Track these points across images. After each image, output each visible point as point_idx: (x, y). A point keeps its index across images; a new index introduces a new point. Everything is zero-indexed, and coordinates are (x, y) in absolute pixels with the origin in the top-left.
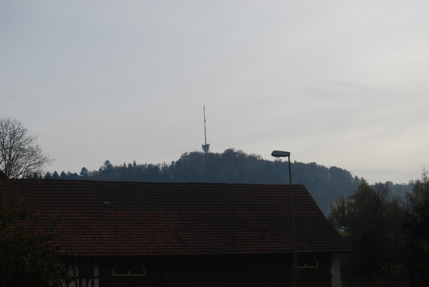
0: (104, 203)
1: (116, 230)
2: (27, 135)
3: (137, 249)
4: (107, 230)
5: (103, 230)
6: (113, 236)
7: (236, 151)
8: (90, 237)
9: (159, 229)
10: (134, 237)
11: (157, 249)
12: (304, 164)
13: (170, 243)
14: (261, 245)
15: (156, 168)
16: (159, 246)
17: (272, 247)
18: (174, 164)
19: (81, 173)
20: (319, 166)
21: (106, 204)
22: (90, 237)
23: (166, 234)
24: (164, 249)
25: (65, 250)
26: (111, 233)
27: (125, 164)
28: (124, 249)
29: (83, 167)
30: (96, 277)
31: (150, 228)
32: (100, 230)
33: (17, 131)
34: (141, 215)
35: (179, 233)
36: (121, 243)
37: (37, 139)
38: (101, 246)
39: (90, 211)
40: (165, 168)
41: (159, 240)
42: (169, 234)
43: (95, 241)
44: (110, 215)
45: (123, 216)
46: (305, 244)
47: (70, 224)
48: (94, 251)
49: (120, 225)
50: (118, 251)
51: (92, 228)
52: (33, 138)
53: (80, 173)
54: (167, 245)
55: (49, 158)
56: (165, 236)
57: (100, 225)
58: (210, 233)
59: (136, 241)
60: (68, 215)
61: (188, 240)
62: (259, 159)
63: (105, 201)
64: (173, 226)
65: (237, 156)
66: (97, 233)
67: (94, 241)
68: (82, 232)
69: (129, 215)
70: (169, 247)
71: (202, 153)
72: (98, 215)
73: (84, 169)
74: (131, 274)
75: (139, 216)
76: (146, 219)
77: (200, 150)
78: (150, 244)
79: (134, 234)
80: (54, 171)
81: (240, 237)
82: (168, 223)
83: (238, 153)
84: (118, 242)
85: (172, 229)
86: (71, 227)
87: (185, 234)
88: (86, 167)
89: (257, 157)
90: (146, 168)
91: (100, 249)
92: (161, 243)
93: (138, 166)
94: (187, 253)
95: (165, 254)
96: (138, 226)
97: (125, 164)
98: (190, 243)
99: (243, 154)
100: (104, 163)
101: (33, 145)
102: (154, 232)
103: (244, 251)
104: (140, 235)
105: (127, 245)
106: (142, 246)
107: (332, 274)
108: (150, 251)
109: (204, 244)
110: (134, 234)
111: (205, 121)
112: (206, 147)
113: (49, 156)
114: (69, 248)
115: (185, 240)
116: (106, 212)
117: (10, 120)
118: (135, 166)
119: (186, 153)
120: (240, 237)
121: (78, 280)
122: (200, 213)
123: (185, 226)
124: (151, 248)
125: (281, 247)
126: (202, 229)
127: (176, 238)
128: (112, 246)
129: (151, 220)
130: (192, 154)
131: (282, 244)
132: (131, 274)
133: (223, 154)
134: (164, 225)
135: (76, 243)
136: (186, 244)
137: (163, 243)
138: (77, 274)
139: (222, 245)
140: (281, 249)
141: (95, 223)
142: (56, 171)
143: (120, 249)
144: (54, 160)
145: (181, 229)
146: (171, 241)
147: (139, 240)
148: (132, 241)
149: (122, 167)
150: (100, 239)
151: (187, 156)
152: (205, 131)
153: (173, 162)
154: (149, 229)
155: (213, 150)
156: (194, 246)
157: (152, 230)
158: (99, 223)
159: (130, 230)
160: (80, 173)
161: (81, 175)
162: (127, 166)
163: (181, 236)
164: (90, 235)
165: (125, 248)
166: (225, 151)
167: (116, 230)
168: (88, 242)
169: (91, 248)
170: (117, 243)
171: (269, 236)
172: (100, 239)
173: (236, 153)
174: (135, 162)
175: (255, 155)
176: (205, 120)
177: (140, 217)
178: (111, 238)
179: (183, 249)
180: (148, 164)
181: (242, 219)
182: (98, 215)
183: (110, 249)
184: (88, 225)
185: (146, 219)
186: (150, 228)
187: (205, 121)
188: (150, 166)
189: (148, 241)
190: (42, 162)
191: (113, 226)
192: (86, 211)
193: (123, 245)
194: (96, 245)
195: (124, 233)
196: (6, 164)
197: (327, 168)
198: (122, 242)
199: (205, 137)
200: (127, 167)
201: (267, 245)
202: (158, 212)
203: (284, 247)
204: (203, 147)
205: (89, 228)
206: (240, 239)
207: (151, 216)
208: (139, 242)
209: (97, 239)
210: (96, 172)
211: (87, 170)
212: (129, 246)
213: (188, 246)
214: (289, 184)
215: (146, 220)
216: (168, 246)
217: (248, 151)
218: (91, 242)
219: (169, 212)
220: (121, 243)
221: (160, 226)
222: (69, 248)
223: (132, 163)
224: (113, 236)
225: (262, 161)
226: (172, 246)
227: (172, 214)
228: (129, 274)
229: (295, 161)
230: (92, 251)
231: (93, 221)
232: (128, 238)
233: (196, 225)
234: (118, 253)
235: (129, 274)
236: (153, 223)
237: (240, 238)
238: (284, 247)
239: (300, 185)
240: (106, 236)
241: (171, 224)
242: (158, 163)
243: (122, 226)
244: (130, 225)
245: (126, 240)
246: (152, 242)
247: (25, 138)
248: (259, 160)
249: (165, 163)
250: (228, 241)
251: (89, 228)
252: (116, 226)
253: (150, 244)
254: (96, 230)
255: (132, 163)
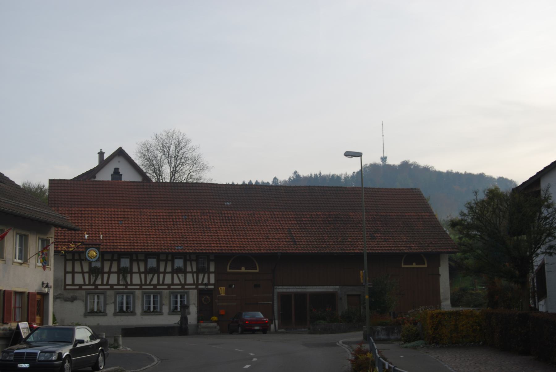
0: (225, 204)
1: (233, 229)
2: (190, 145)
3: (250, 247)
4: (224, 229)
5: (221, 229)
6: (229, 235)
7: (411, 162)
8: (208, 236)
9: (274, 229)
10: (249, 236)
11: (269, 247)
12: (394, 165)
13: (283, 242)
14: (370, 244)
15: (338, 178)
16: (271, 244)
17: (381, 247)
18: (355, 174)
19: (273, 182)
20: (488, 176)
21: (227, 205)
22: (208, 236)
23: (279, 234)
24: (275, 247)
25: (182, 247)
26: (228, 232)
27: (311, 175)
28: (237, 247)
29: (274, 177)
30: (212, 273)
31: (266, 227)
32: (217, 229)
33: (181, 141)
34: (259, 216)
35: (293, 233)
36: (235, 241)
37: (199, 149)
38: (217, 244)
39: (210, 211)
40: (347, 178)
41: (272, 239)
42: (282, 234)
43: (212, 238)
44: (229, 215)
45: (241, 216)
46: (413, 244)
47: (191, 223)
48: (209, 248)
49: (237, 224)
50: (232, 248)
51: (211, 226)
52: (196, 147)
53: (272, 182)
54: (280, 243)
55: (208, 166)
56: (278, 235)
57: (219, 224)
58: (323, 233)
59: (250, 239)
60: (190, 214)
61: (300, 239)
62: (432, 169)
63: (226, 202)
64: (288, 226)
65: (412, 167)
66: (215, 231)
67: (210, 239)
68: (200, 230)
69: (247, 216)
70: (281, 245)
71: (380, 164)
72: (217, 215)
73: (275, 178)
74: (245, 269)
75: (256, 216)
76: (263, 219)
77: (379, 162)
78: (263, 243)
79: (249, 233)
80: (249, 180)
81: (351, 236)
82: (283, 223)
83: (412, 165)
84: (234, 240)
85: (286, 229)
86: (191, 226)
87: (298, 234)
88: (277, 177)
89: (430, 168)
90: (330, 178)
91: (215, 246)
92: (273, 241)
93: (323, 176)
94: (297, 251)
95: (276, 251)
96: (255, 226)
97: (311, 175)
98: (301, 242)
99: (418, 165)
100: (293, 173)
101: (195, 154)
102: (269, 231)
103: (353, 250)
104: (255, 233)
105: (241, 243)
106: (255, 244)
107: (440, 273)
108: (262, 249)
109: (315, 243)
110: (249, 233)
111: (383, 135)
112: (384, 159)
113: (208, 163)
114: (186, 245)
115: (297, 239)
116: (226, 212)
117: (175, 132)
118: (321, 176)
119: (366, 165)
120: (351, 236)
121: (195, 275)
122: (315, 214)
123: (299, 226)
124: (264, 246)
125: (390, 247)
126: (315, 229)
127: (289, 237)
128: (226, 244)
129: (268, 220)
130: (371, 165)
131: (391, 244)
132: (245, 269)
133: (399, 166)
134: (279, 224)
135: (193, 241)
136: (298, 243)
137: (276, 241)
138: (195, 270)
139: (332, 244)
140: (389, 248)
141: (214, 222)
142: (251, 180)
143: (234, 247)
144: (213, 167)
145: (295, 229)
146: (284, 240)
147: (253, 239)
148: (247, 239)
149: (308, 177)
150: (216, 237)
151: (367, 167)
152: (383, 145)
153: (354, 172)
154: (265, 228)
155: (389, 162)
156: (304, 244)
157: (267, 229)
158: (217, 222)
159: (246, 230)
160: (272, 182)
161: (273, 183)
162: (313, 176)
163: (294, 235)
164: (207, 233)
165: (239, 245)
166: (401, 163)
167: (233, 229)
168: (205, 239)
169: (206, 245)
170: (232, 241)
171: (380, 236)
172: (216, 237)
173: (411, 165)
174: (320, 172)
175: (428, 166)
176: (384, 134)
177: (258, 217)
178: (227, 236)
179: (294, 247)
180: (332, 174)
181: (355, 220)
182: (217, 215)
183: (224, 247)
184: (207, 224)
185: (263, 219)
186: (266, 227)
187: (383, 135)
188: (333, 176)
189: (262, 240)
190: (204, 170)
191: (230, 226)
192: (207, 211)
193: (237, 243)
194: (212, 242)
195: (240, 232)
196: (172, 171)
197: (494, 179)
198: (236, 240)
199: (384, 150)
200: (313, 177)
201: (376, 244)
202: (275, 213)
203: (392, 247)
204: (382, 158)
205: (208, 227)
206: (350, 239)
207: (268, 216)
208: (253, 240)
209: (214, 237)
210: (286, 181)
211: (278, 180)
212: (243, 244)
213: (299, 244)
214: (360, 186)
215: (262, 220)
216: (280, 244)
217: (422, 162)
218: (207, 239)
219: (286, 212)
220: (235, 241)
221: (276, 226)
222: (186, 245)
223: (318, 173)
224: (229, 235)
225: (435, 171)
226: (284, 244)
227: (288, 215)
228: (243, 270)
229: (465, 172)
230: (207, 248)
231: (212, 221)
232: (243, 236)
233: (310, 225)
234: (231, 250)
235: (243, 270)
236: (269, 223)
237: (351, 238)
238: (392, 247)
239: (415, 189)
240: (222, 234)
241: (286, 224)
242: (340, 173)
243: (239, 226)
244: (247, 224)
245: (241, 239)
246: (265, 240)
247: (189, 147)
248: (432, 171)
249: (346, 173)
250: (338, 241)
251: (208, 227)
252: (233, 226)
253: (263, 243)
254: (214, 229)
255: (318, 173)
